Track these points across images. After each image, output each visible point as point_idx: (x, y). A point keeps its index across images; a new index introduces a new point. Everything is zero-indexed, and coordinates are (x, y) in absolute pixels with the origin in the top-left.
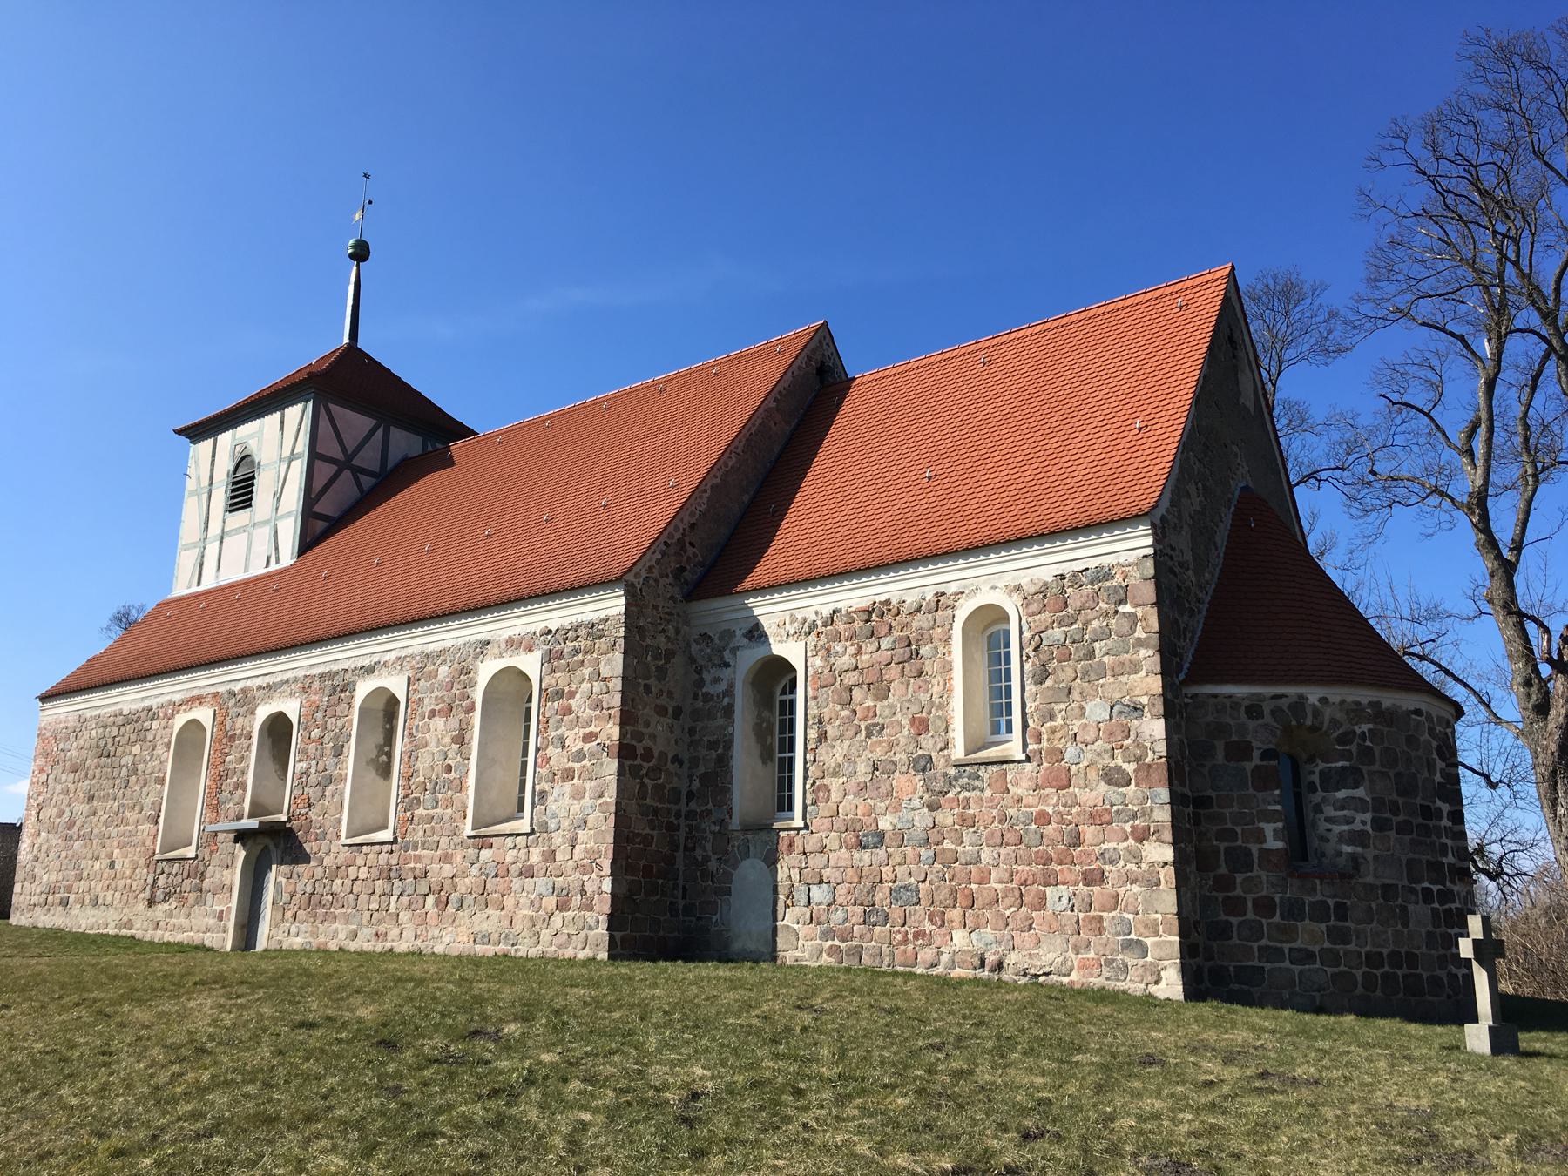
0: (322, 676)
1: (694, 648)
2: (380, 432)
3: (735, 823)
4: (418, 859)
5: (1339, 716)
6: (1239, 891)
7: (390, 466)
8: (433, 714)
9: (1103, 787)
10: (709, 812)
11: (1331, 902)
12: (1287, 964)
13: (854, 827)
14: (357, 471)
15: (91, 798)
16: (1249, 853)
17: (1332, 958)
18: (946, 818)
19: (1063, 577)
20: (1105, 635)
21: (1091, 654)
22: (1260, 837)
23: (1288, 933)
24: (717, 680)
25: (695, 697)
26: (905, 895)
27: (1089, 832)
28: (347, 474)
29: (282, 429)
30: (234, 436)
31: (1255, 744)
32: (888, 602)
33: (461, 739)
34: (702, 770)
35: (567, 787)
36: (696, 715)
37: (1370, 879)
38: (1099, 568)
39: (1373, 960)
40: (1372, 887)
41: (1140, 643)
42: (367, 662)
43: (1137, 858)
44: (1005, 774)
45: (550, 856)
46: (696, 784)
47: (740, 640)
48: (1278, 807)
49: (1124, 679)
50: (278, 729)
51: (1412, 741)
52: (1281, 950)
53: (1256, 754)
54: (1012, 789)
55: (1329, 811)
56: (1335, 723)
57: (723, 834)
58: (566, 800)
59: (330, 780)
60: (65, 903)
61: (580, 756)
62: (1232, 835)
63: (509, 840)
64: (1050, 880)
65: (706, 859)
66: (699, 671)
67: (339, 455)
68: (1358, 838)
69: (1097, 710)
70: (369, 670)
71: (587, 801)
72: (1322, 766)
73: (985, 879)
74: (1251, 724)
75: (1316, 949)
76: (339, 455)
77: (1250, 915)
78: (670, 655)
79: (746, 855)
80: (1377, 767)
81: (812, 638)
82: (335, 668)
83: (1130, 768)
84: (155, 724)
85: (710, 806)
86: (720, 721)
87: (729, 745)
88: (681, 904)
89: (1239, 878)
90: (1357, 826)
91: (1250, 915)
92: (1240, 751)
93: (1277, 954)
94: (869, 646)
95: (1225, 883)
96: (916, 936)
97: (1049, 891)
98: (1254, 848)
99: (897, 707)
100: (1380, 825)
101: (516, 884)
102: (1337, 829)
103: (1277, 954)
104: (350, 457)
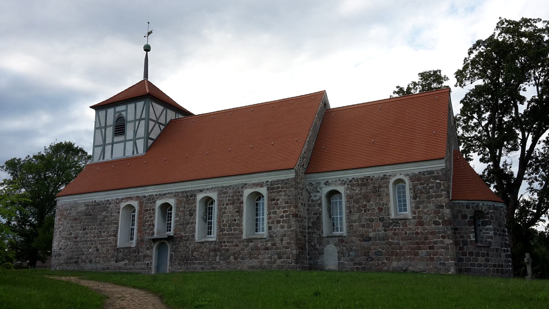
0: (182, 192)
1: (307, 187)
2: (165, 111)
3: (324, 235)
4: (226, 246)
5: (486, 208)
6: (465, 250)
7: (168, 122)
8: (227, 204)
9: (433, 226)
10: (315, 232)
13: (362, 235)
14: (160, 124)
15: (84, 229)
16: (467, 241)
17: (486, 266)
18: (390, 233)
19: (420, 173)
20: (432, 188)
21: (428, 192)
22: (470, 237)
23: (476, 260)
24: (316, 196)
25: (309, 200)
26: (378, 253)
29: (135, 109)
30: (115, 110)
32: (369, 177)
33: (240, 212)
34: (312, 220)
36: (309, 205)
37: (493, 247)
38: (430, 171)
39: (494, 266)
40: (493, 249)
41: (442, 190)
42: (200, 188)
43: (442, 242)
45: (274, 244)
46: (310, 225)
47: (322, 185)
48: (31, 201)
49: (438, 199)
50: (166, 207)
51: (500, 214)
52: (475, 264)
53: (468, 217)
54: (408, 226)
55: (484, 231)
56: (486, 210)
57: (321, 238)
58: (279, 229)
60: (77, 262)
61: (282, 217)
62: (463, 237)
63: (260, 241)
64: (420, 248)
65: (315, 245)
66: (309, 193)
67: (155, 119)
68: (491, 237)
69: (431, 206)
70: (201, 191)
71: (286, 229)
72: (482, 220)
73: (401, 248)
74: (467, 210)
75: (482, 263)
76: (155, 119)
78: (303, 188)
79: (328, 243)
81: (346, 186)
82: (187, 190)
83: (441, 221)
84: (111, 206)
85: (315, 230)
86: (317, 207)
87: (321, 214)
88: (308, 257)
89: (465, 247)
90: (490, 234)
91: (468, 256)
92: (464, 217)
93: (474, 265)
94: (364, 188)
95: (461, 249)
96: (382, 264)
97: (419, 251)
98: (469, 240)
99: (372, 204)
100: (495, 234)
101: (262, 252)
102: (486, 235)
103: (474, 265)
104: (158, 119)
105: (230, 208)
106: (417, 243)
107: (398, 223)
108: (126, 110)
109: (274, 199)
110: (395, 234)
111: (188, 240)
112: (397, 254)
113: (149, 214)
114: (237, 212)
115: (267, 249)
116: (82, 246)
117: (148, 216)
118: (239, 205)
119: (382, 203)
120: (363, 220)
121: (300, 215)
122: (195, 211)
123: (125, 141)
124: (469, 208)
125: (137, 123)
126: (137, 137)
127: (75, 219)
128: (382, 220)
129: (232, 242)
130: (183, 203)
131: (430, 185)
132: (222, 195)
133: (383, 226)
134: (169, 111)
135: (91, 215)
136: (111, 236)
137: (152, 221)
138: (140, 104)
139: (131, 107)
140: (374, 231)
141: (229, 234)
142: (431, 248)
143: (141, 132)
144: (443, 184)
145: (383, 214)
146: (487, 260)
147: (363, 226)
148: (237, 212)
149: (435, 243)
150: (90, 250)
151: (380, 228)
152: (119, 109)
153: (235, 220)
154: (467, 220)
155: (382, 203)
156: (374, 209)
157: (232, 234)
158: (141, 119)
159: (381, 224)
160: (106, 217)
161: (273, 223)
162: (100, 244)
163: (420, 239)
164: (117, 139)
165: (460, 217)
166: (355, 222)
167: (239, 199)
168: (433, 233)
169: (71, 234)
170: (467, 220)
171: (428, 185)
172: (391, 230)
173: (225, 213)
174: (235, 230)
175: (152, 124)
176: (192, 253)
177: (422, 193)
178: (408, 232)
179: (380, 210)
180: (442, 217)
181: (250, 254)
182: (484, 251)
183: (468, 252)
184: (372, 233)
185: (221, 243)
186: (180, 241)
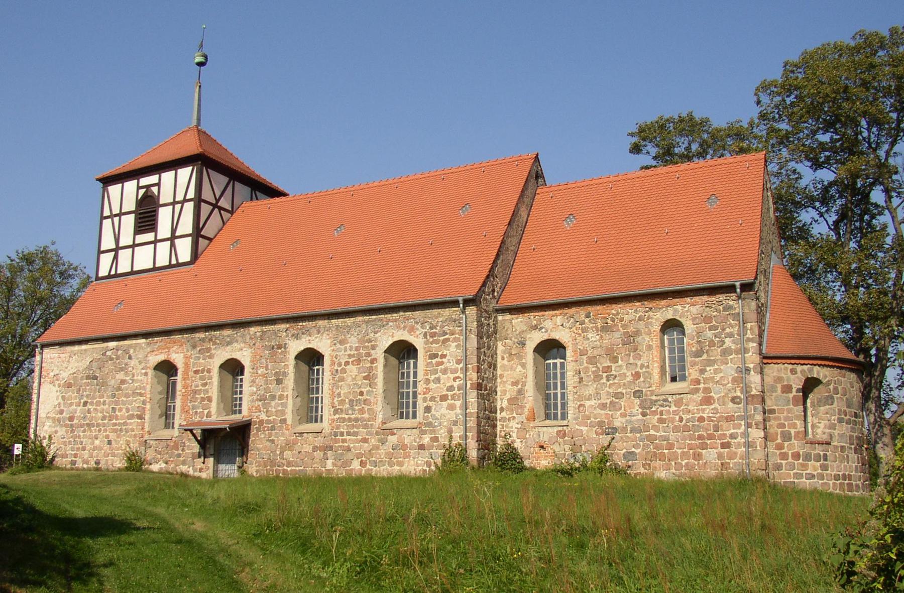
4: (344, 441)
8: (347, 363)
9: (731, 405)
10: (514, 418)
11: (822, 453)
12: (804, 480)
13: (601, 424)
15: (85, 404)
16: (790, 433)
17: (821, 477)
23: (804, 467)
27: (723, 424)
28: (216, 210)
31: (794, 386)
33: (370, 378)
35: (445, 404)
37: (835, 443)
39: (837, 477)
40: (836, 447)
41: (749, 340)
44: (682, 399)
53: (794, 390)
58: (444, 411)
59: (262, 399)
61: (451, 388)
64: (704, 446)
67: (214, 202)
73: (670, 447)
74: (792, 377)
75: (815, 473)
76: (214, 202)
77: (790, 460)
80: (839, 396)
85: (515, 415)
89: (786, 444)
91: (790, 460)
97: (704, 451)
99: (622, 368)
100: (840, 421)
104: (218, 201)
105: (353, 369)
106: (700, 437)
107: (666, 400)
108: (158, 185)
109: (435, 356)
110: (661, 421)
111: (273, 428)
112: (662, 457)
113: (202, 378)
114: (365, 378)
115: (422, 447)
116: (82, 434)
117: (200, 382)
118: (369, 365)
119: (639, 363)
120: (604, 396)
121: (486, 386)
122: (285, 374)
123: (155, 242)
124: (796, 373)
125: (178, 207)
126: (177, 234)
127: (69, 386)
128: (638, 394)
129: (356, 434)
130: (263, 360)
131: (728, 330)
132: (338, 345)
133: (641, 406)
134: (238, 185)
135: (96, 378)
136: (131, 417)
137: (207, 391)
138: (185, 173)
139: (168, 177)
140: (623, 415)
141: (350, 420)
142: (724, 446)
143: (186, 225)
144: (751, 329)
145: (640, 385)
146: (824, 468)
147: (603, 406)
148: (365, 378)
149: (733, 436)
150: (97, 442)
151: (634, 411)
152: (145, 181)
153: (361, 394)
154: (791, 395)
155: (639, 363)
156: (625, 374)
157: (356, 420)
158: (185, 200)
159: (637, 401)
160: (123, 382)
161: (433, 399)
162: (115, 431)
163: (707, 430)
164: (141, 238)
165: (779, 390)
166: (589, 399)
167: (369, 355)
168: (729, 419)
169: (61, 412)
170: (791, 395)
171: (724, 329)
172: (654, 413)
173: (342, 379)
174: (362, 411)
175: (205, 209)
176: (282, 453)
177: (712, 344)
178: (685, 417)
179: (637, 375)
180: (746, 390)
181: (390, 456)
182: (819, 450)
183: (790, 453)
184: (620, 419)
185: (336, 435)
186: (258, 430)
